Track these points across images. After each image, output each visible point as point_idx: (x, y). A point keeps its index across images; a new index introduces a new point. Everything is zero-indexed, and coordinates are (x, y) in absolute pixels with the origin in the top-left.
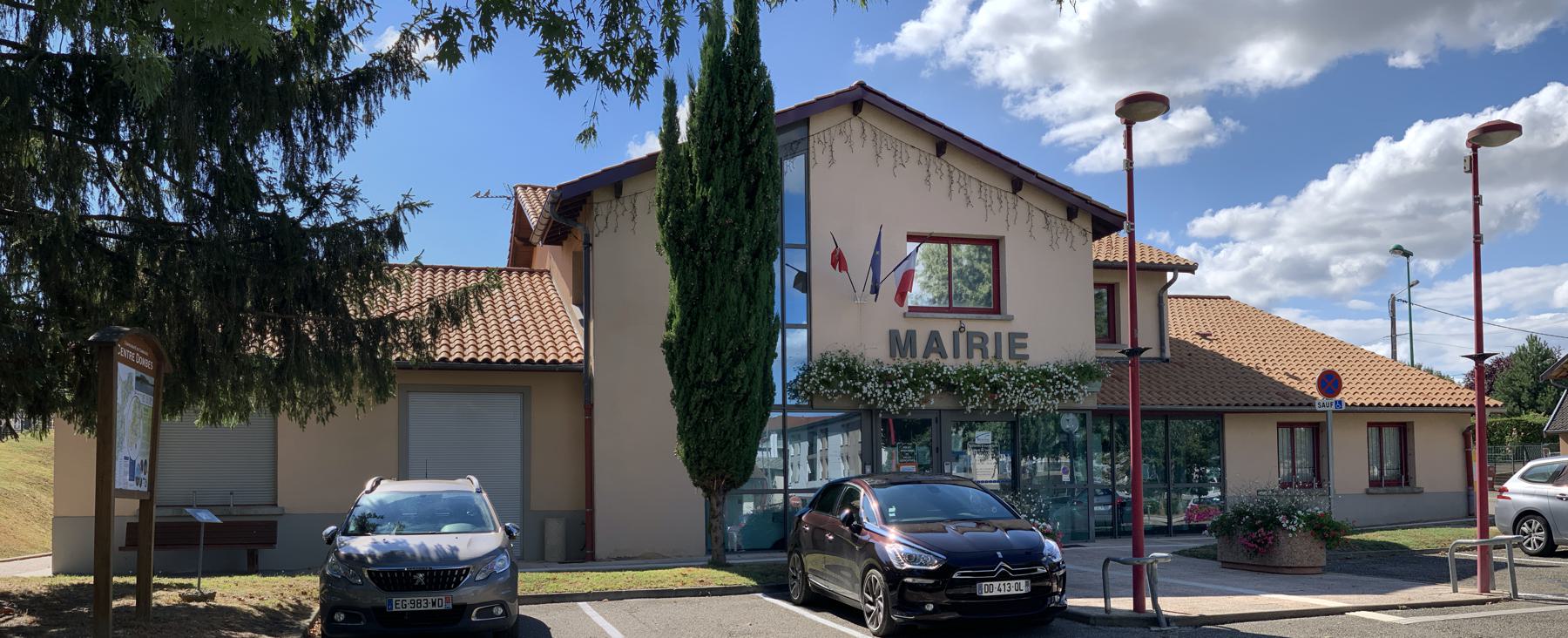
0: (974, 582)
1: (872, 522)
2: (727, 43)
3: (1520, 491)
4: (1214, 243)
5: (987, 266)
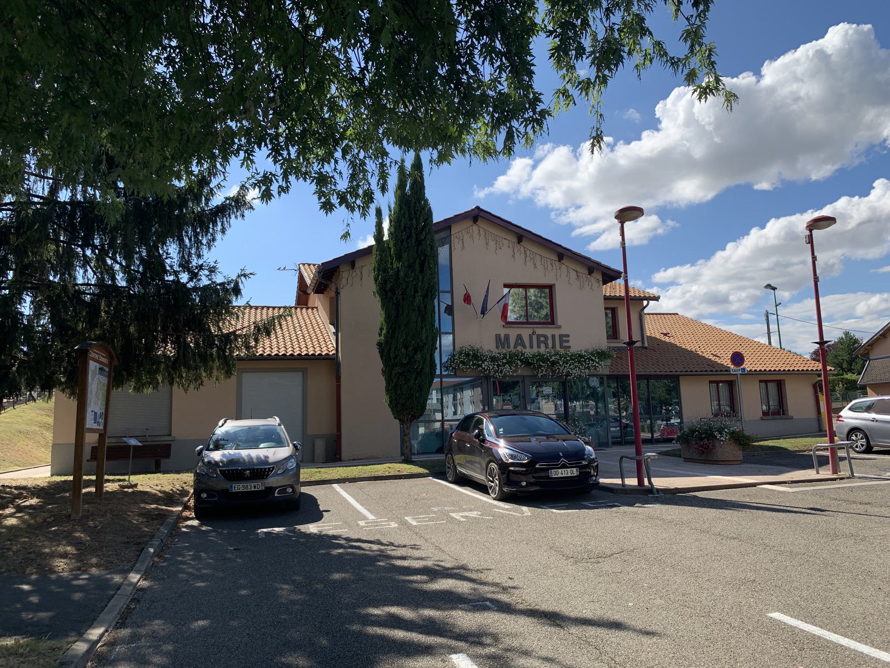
0: (547, 470)
2: (408, 188)
3: (849, 417)
4: (664, 286)
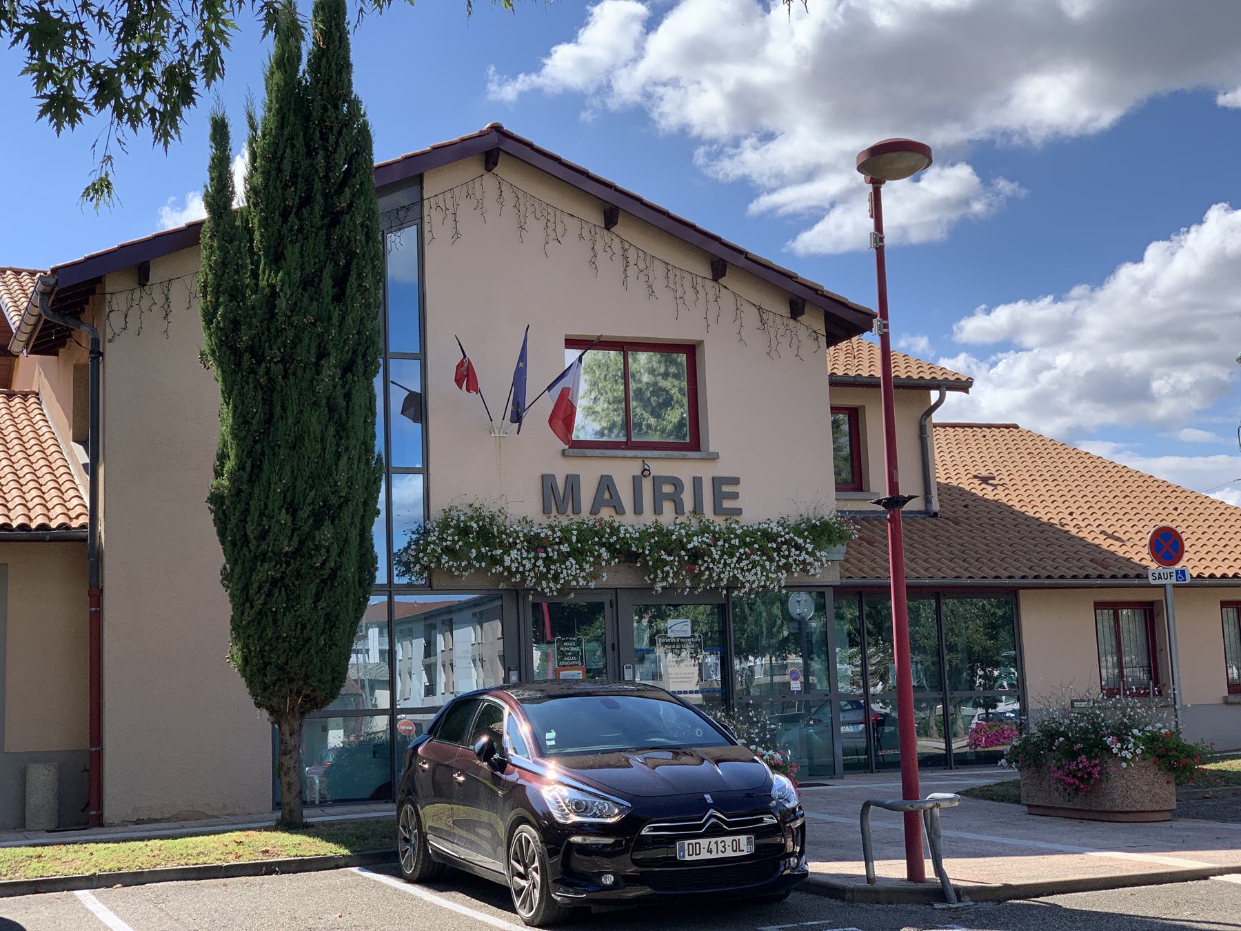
0: (671, 841)
1: (522, 754)
2: (303, 66)
4: (988, 352)
5: (676, 383)
